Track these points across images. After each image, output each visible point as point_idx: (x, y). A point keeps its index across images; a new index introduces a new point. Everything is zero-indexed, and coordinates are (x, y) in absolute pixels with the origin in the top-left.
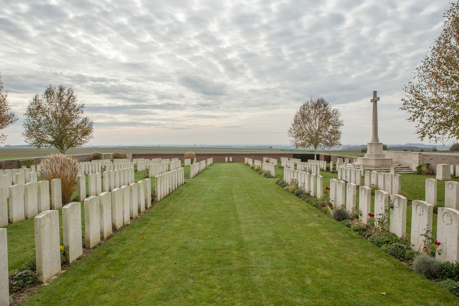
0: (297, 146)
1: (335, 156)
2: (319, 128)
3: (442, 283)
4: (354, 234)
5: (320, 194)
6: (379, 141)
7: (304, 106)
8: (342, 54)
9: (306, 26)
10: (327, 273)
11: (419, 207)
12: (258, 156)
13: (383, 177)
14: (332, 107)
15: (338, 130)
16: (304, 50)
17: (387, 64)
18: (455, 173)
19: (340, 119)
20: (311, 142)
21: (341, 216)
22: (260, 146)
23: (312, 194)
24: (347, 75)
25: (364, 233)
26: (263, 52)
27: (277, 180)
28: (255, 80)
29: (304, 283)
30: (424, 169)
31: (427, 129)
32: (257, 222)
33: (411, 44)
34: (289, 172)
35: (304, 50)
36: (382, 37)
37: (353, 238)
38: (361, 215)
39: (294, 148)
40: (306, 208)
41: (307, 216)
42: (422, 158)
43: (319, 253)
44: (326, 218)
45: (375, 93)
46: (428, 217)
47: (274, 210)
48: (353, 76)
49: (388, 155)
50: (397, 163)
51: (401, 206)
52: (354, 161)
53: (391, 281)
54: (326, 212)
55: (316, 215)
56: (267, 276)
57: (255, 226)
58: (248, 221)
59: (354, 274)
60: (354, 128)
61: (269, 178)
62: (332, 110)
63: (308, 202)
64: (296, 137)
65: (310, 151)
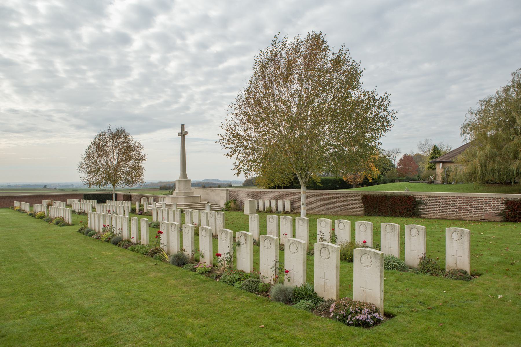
0: (90, 184)
1: (136, 196)
2: (118, 163)
3: (298, 304)
4: (203, 277)
5: (145, 239)
6: (187, 178)
7: (100, 136)
8: (130, 79)
9: (86, 40)
10: (202, 322)
11: (266, 241)
12: (34, 199)
13: (205, 215)
14: (134, 138)
15: (140, 165)
16: (84, 67)
17: (180, 97)
18: (258, 208)
19: (142, 153)
20: (108, 180)
21: (180, 261)
22: (29, 185)
23: (134, 241)
24: (137, 103)
25: (211, 275)
26: (27, 62)
27: (79, 227)
28: (16, 97)
29: (185, 336)
30: (232, 205)
31: (241, 166)
32: (85, 283)
33: (201, 78)
34: (97, 216)
35: (84, 67)
36: (173, 67)
37: (204, 281)
38: (203, 257)
39: (86, 187)
40: (136, 258)
41: (142, 266)
42: (229, 194)
43: (181, 303)
44: (163, 266)
45: (183, 126)
46: (276, 249)
47: (98, 264)
48: (144, 105)
49: (197, 192)
50: (205, 200)
51: (249, 242)
52: (159, 200)
53: (261, 313)
54: (161, 259)
55: (151, 264)
56: (141, 341)
57: (87, 288)
58: (73, 283)
59: (227, 316)
60: (158, 164)
61: (63, 226)
62: (133, 142)
63: (133, 250)
64: (89, 173)
65: (99, 190)
